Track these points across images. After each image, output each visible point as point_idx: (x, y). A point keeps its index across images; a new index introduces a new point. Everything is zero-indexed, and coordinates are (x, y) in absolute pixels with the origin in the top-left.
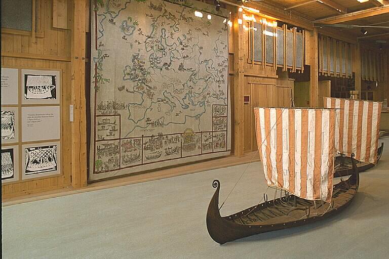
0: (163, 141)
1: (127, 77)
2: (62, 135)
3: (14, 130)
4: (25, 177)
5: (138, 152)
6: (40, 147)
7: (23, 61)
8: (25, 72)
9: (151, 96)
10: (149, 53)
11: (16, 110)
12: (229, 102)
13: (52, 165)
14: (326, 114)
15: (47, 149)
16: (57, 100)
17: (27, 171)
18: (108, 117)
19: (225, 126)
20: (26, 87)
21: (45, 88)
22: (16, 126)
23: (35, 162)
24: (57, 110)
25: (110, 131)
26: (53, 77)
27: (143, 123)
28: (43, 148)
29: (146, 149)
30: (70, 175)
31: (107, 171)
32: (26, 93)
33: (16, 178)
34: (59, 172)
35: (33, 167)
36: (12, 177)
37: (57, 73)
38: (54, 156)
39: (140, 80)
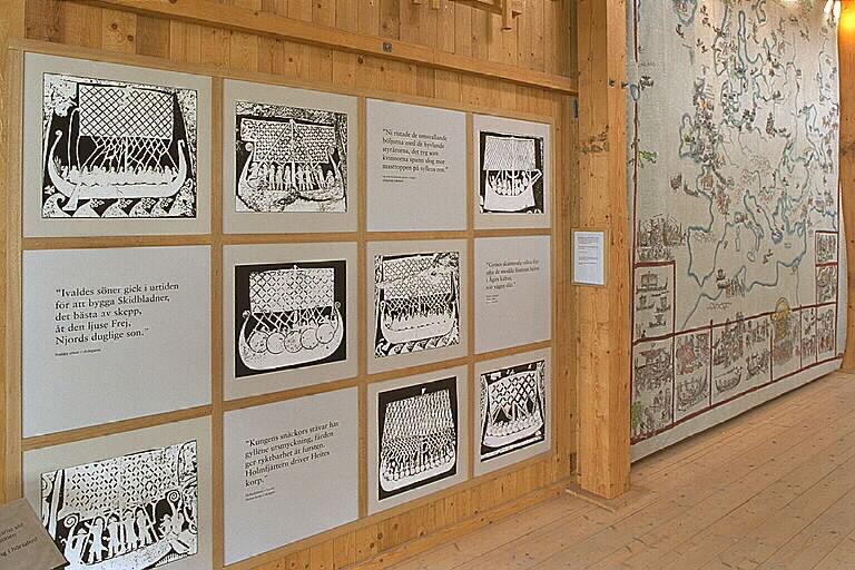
0: (745, 335)
1: (686, 148)
2: (557, 327)
3: (457, 317)
4: (483, 468)
5: (699, 374)
6: (511, 369)
7: (240, 48)
8: (483, 123)
9: (724, 203)
10: (722, 79)
11: (459, 246)
12: (842, 224)
13: (529, 425)
14: (638, 434)
15: (525, 374)
16: (543, 219)
17: (485, 449)
18: (654, 270)
19: (833, 291)
20: (483, 173)
21: (521, 177)
22: (462, 302)
23: (502, 417)
24: (543, 248)
25: (658, 309)
26: (538, 142)
27: (711, 287)
28: (518, 370)
29: (718, 361)
30: (568, 452)
31: (650, 435)
32: (483, 193)
33: (461, 476)
34: (547, 445)
35: (498, 436)
36: (453, 472)
37: (544, 131)
38: (538, 397)
39: (706, 159)
